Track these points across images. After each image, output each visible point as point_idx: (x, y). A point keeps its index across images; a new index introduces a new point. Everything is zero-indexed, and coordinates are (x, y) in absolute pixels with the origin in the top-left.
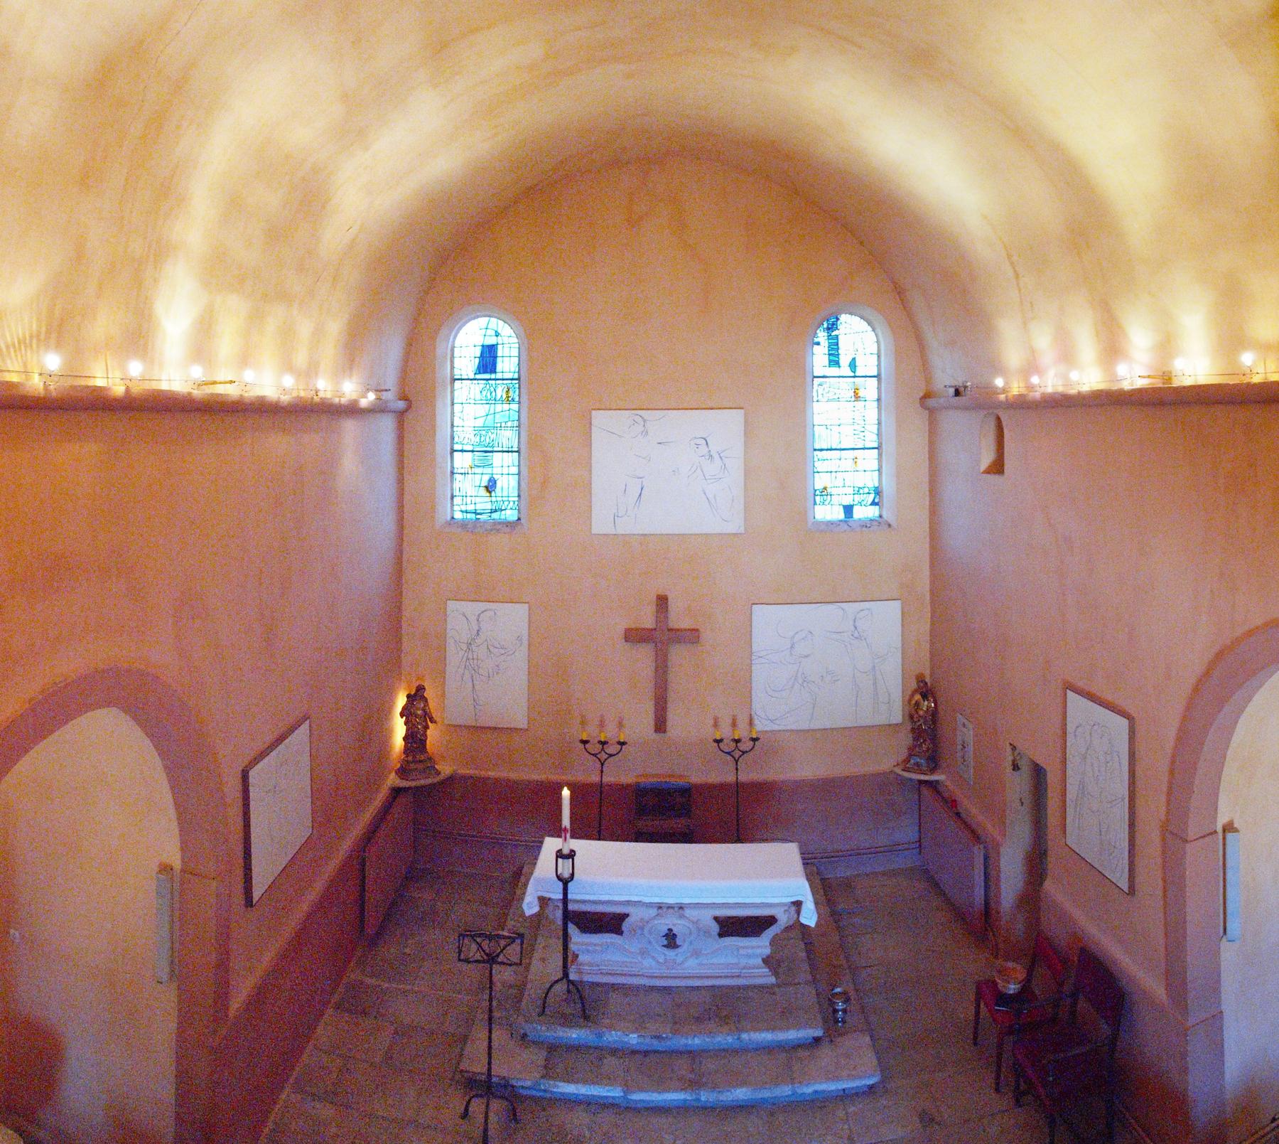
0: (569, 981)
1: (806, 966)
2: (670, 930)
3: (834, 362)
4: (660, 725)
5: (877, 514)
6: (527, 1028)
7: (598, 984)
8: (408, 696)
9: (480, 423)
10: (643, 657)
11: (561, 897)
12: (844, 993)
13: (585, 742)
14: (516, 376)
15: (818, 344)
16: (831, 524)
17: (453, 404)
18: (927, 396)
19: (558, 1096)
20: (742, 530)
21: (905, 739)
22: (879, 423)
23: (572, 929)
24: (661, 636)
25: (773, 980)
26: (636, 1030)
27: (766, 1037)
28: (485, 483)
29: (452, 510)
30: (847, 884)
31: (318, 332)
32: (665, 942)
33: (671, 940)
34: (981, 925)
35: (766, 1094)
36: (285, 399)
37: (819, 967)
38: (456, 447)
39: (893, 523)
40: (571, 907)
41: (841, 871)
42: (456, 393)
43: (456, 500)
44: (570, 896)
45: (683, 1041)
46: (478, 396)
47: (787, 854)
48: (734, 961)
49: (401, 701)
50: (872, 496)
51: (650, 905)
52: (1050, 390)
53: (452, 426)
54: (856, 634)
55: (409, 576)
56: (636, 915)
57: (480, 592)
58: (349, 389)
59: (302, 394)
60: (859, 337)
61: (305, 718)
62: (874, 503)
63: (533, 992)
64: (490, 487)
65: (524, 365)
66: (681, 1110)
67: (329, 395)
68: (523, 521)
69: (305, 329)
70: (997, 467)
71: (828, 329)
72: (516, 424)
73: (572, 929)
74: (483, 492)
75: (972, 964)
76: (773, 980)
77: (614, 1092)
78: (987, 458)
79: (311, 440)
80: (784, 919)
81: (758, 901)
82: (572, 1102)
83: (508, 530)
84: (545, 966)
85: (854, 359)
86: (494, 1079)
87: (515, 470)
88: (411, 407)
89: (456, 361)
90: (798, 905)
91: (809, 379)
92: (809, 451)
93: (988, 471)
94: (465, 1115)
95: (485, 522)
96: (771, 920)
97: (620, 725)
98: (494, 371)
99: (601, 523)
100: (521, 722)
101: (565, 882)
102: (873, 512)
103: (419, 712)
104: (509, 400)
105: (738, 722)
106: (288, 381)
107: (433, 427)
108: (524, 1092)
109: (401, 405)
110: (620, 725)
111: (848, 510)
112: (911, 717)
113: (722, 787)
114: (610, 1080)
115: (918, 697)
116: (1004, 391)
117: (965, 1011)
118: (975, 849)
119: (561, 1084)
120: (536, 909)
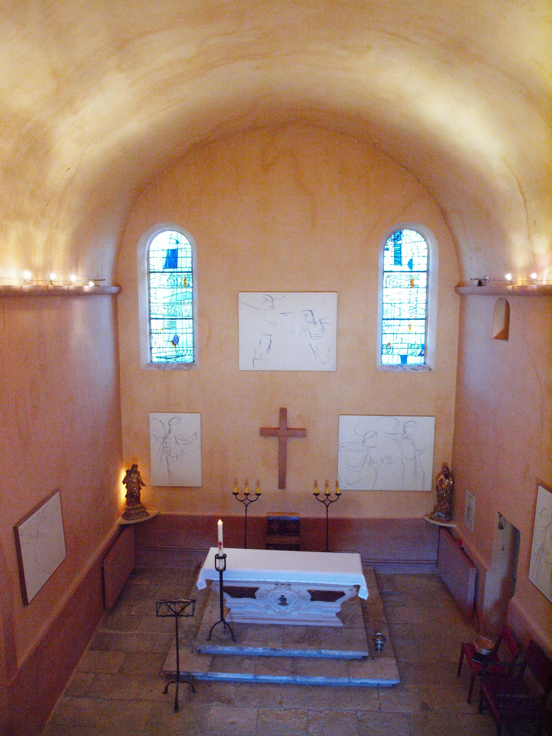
0: (225, 623)
1: (361, 619)
2: (283, 596)
3: (398, 260)
4: (282, 484)
5: (423, 361)
6: (201, 647)
7: (243, 624)
8: (127, 471)
9: (167, 300)
10: (272, 444)
11: (218, 579)
12: (382, 636)
13: (236, 494)
14: (190, 270)
15: (387, 249)
16: (392, 366)
17: (149, 288)
18: (460, 285)
19: (218, 679)
20: (334, 369)
21: (433, 501)
22: (427, 303)
23: (226, 596)
24: (282, 432)
25: (341, 625)
26: (262, 646)
27: (337, 653)
28: (171, 339)
29: (151, 357)
30: (390, 579)
31: (50, 244)
32: (280, 602)
33: (283, 601)
34: (471, 613)
35: (334, 681)
36: (26, 287)
37: (368, 623)
38: (152, 316)
39: (432, 366)
40: (225, 584)
41: (385, 571)
42: (151, 281)
43: (154, 350)
44: (224, 579)
45: (288, 652)
46: (166, 283)
47: (353, 560)
48: (320, 613)
49: (123, 475)
50: (420, 350)
51: (271, 583)
52: (544, 283)
53: (150, 302)
54: (405, 436)
55: (124, 400)
56: (263, 588)
57: (170, 407)
58: (75, 279)
59: (41, 283)
60: (415, 245)
61: (58, 490)
62: (420, 355)
63: (205, 628)
64: (175, 342)
65: (195, 262)
66: (286, 684)
67: (61, 284)
68: (196, 363)
69: (39, 238)
70: (504, 335)
71: (394, 239)
72: (191, 301)
73: (226, 596)
74: (170, 344)
75: (464, 634)
76: (341, 625)
77: (249, 677)
78: (498, 329)
79: (48, 316)
80: (349, 594)
81: (334, 583)
82: (227, 682)
83: (186, 368)
84: (211, 614)
85: (411, 260)
86: (181, 673)
87: (191, 331)
88: (121, 291)
89: (151, 261)
90: (358, 587)
91: (380, 272)
92: (379, 320)
93: (497, 338)
94: (166, 691)
95: (172, 364)
96: (342, 594)
97: (258, 484)
98: (176, 267)
99: (245, 364)
100: (197, 482)
101: (221, 572)
102: (420, 360)
103: (134, 480)
104: (186, 286)
105: (329, 484)
106: (28, 275)
107: (137, 302)
108: (199, 678)
109: (114, 289)
110: (258, 484)
111: (404, 358)
112: (437, 488)
113: (316, 522)
114: (246, 671)
115: (442, 477)
116: (511, 283)
117: (455, 657)
118: (471, 570)
119: (219, 673)
120: (204, 586)
